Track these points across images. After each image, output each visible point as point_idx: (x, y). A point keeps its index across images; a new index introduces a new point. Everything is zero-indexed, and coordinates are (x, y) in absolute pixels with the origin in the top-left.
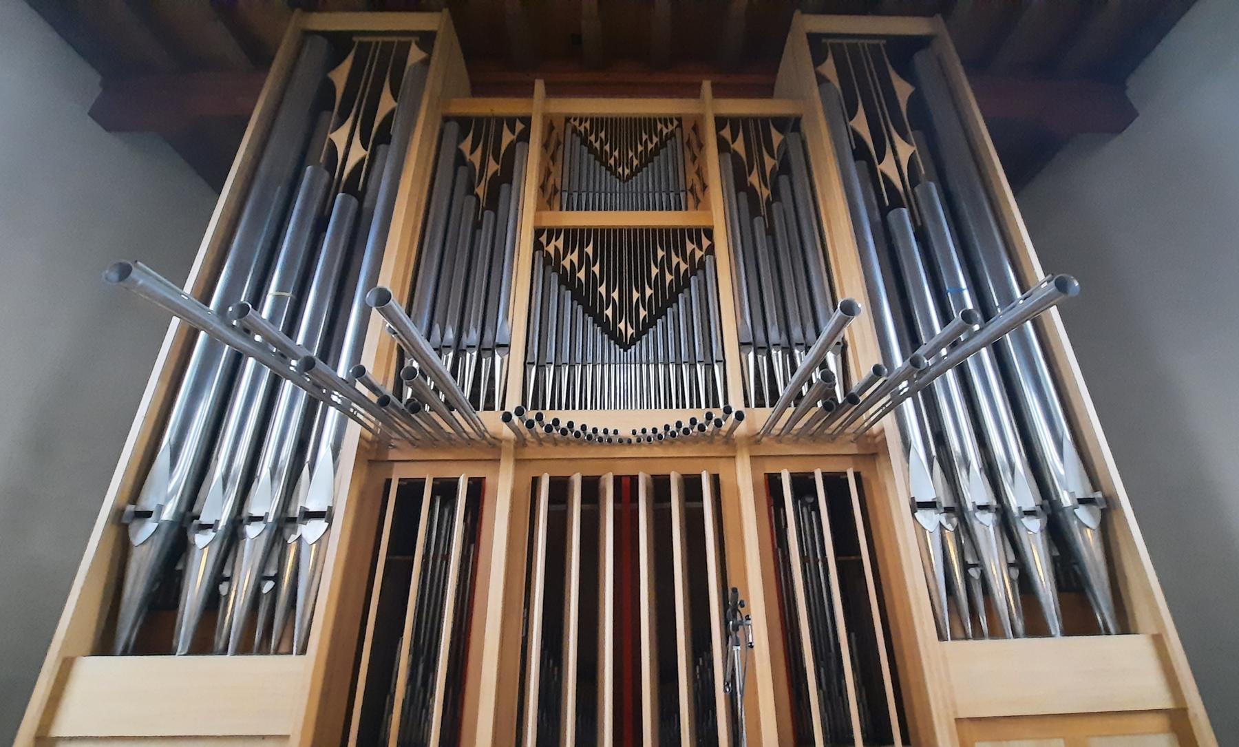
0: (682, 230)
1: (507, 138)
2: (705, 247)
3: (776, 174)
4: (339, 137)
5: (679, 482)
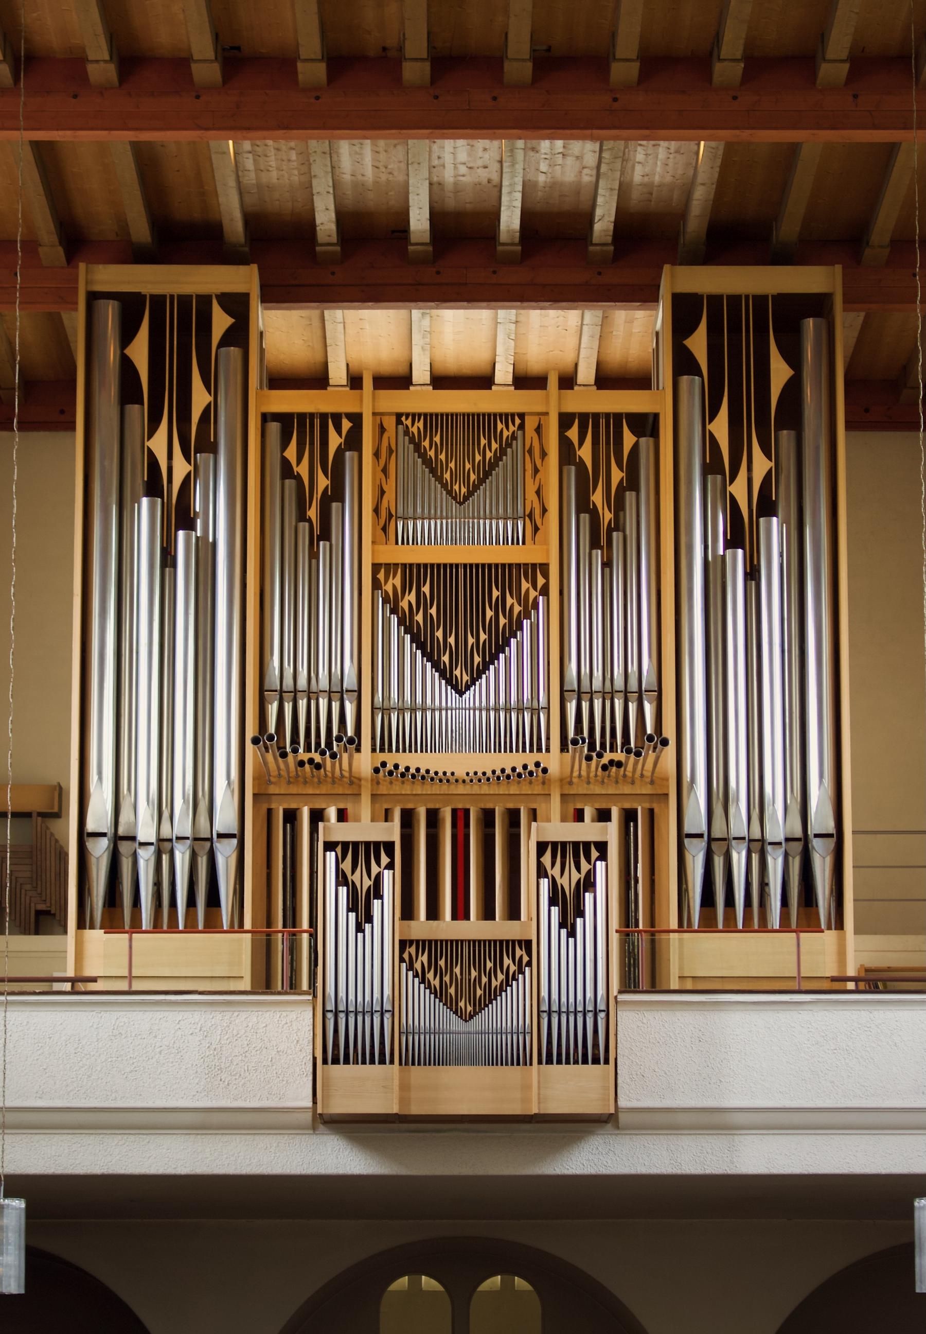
0: (495, 415)
1: (335, 441)
2: (539, 586)
3: (621, 489)
4: (158, 444)
5: (503, 815)
